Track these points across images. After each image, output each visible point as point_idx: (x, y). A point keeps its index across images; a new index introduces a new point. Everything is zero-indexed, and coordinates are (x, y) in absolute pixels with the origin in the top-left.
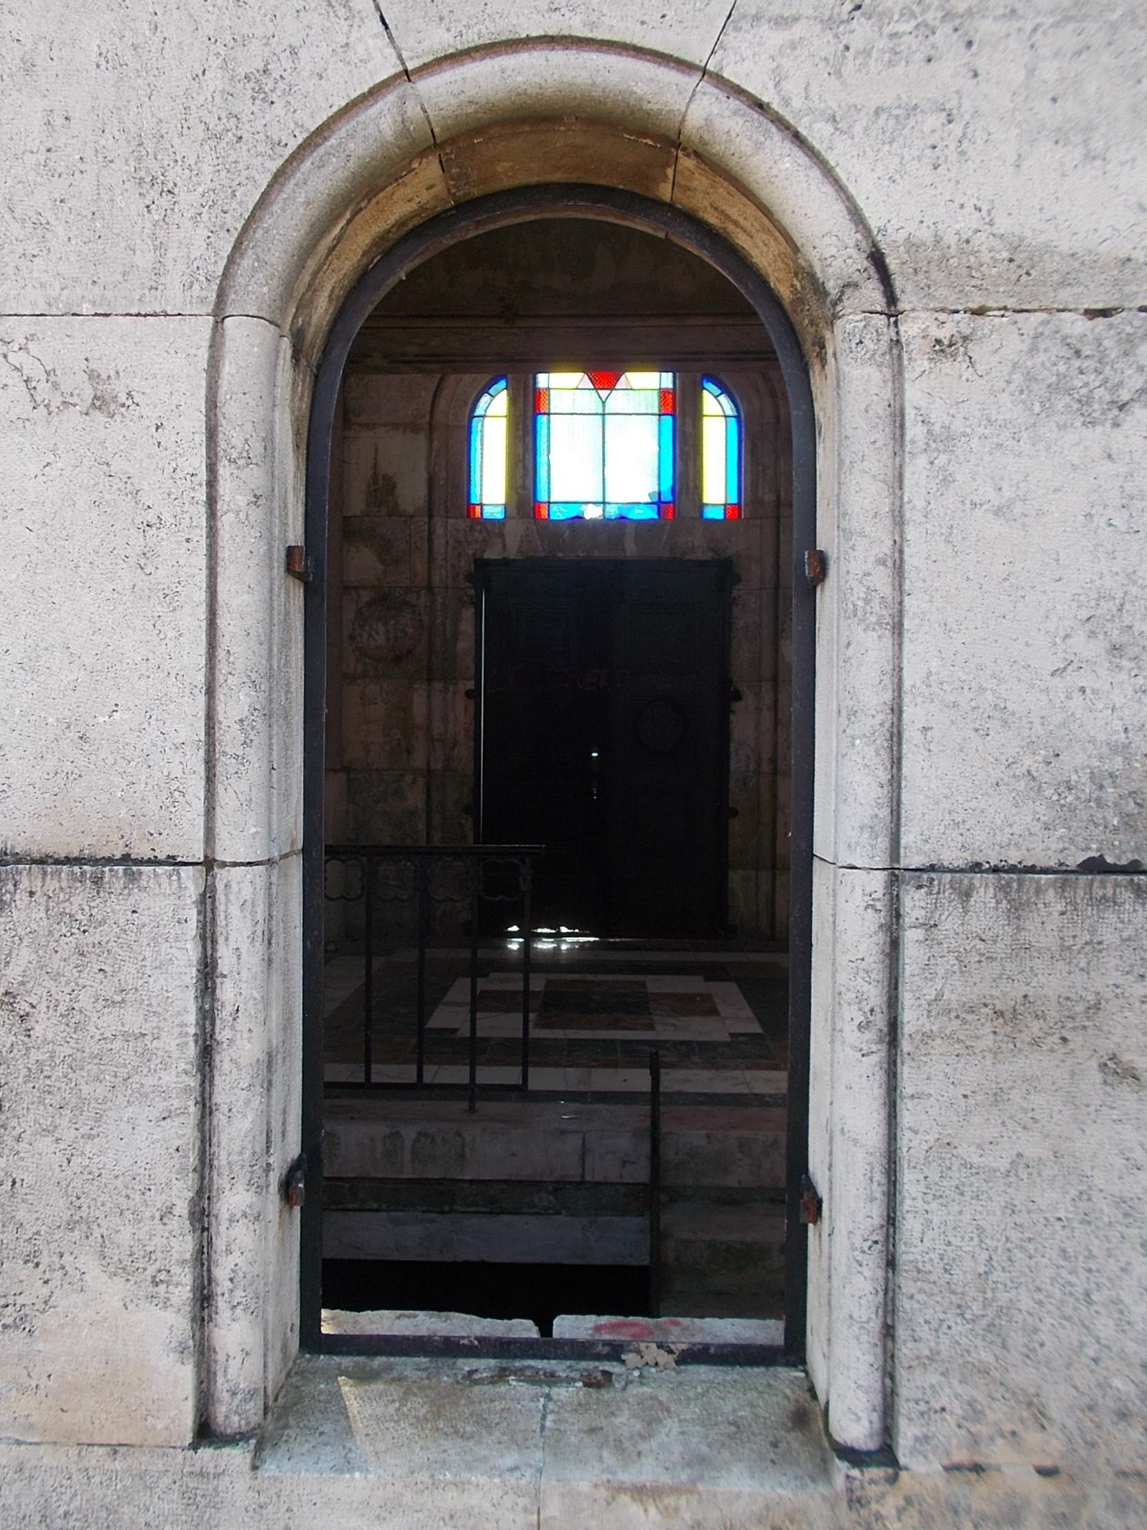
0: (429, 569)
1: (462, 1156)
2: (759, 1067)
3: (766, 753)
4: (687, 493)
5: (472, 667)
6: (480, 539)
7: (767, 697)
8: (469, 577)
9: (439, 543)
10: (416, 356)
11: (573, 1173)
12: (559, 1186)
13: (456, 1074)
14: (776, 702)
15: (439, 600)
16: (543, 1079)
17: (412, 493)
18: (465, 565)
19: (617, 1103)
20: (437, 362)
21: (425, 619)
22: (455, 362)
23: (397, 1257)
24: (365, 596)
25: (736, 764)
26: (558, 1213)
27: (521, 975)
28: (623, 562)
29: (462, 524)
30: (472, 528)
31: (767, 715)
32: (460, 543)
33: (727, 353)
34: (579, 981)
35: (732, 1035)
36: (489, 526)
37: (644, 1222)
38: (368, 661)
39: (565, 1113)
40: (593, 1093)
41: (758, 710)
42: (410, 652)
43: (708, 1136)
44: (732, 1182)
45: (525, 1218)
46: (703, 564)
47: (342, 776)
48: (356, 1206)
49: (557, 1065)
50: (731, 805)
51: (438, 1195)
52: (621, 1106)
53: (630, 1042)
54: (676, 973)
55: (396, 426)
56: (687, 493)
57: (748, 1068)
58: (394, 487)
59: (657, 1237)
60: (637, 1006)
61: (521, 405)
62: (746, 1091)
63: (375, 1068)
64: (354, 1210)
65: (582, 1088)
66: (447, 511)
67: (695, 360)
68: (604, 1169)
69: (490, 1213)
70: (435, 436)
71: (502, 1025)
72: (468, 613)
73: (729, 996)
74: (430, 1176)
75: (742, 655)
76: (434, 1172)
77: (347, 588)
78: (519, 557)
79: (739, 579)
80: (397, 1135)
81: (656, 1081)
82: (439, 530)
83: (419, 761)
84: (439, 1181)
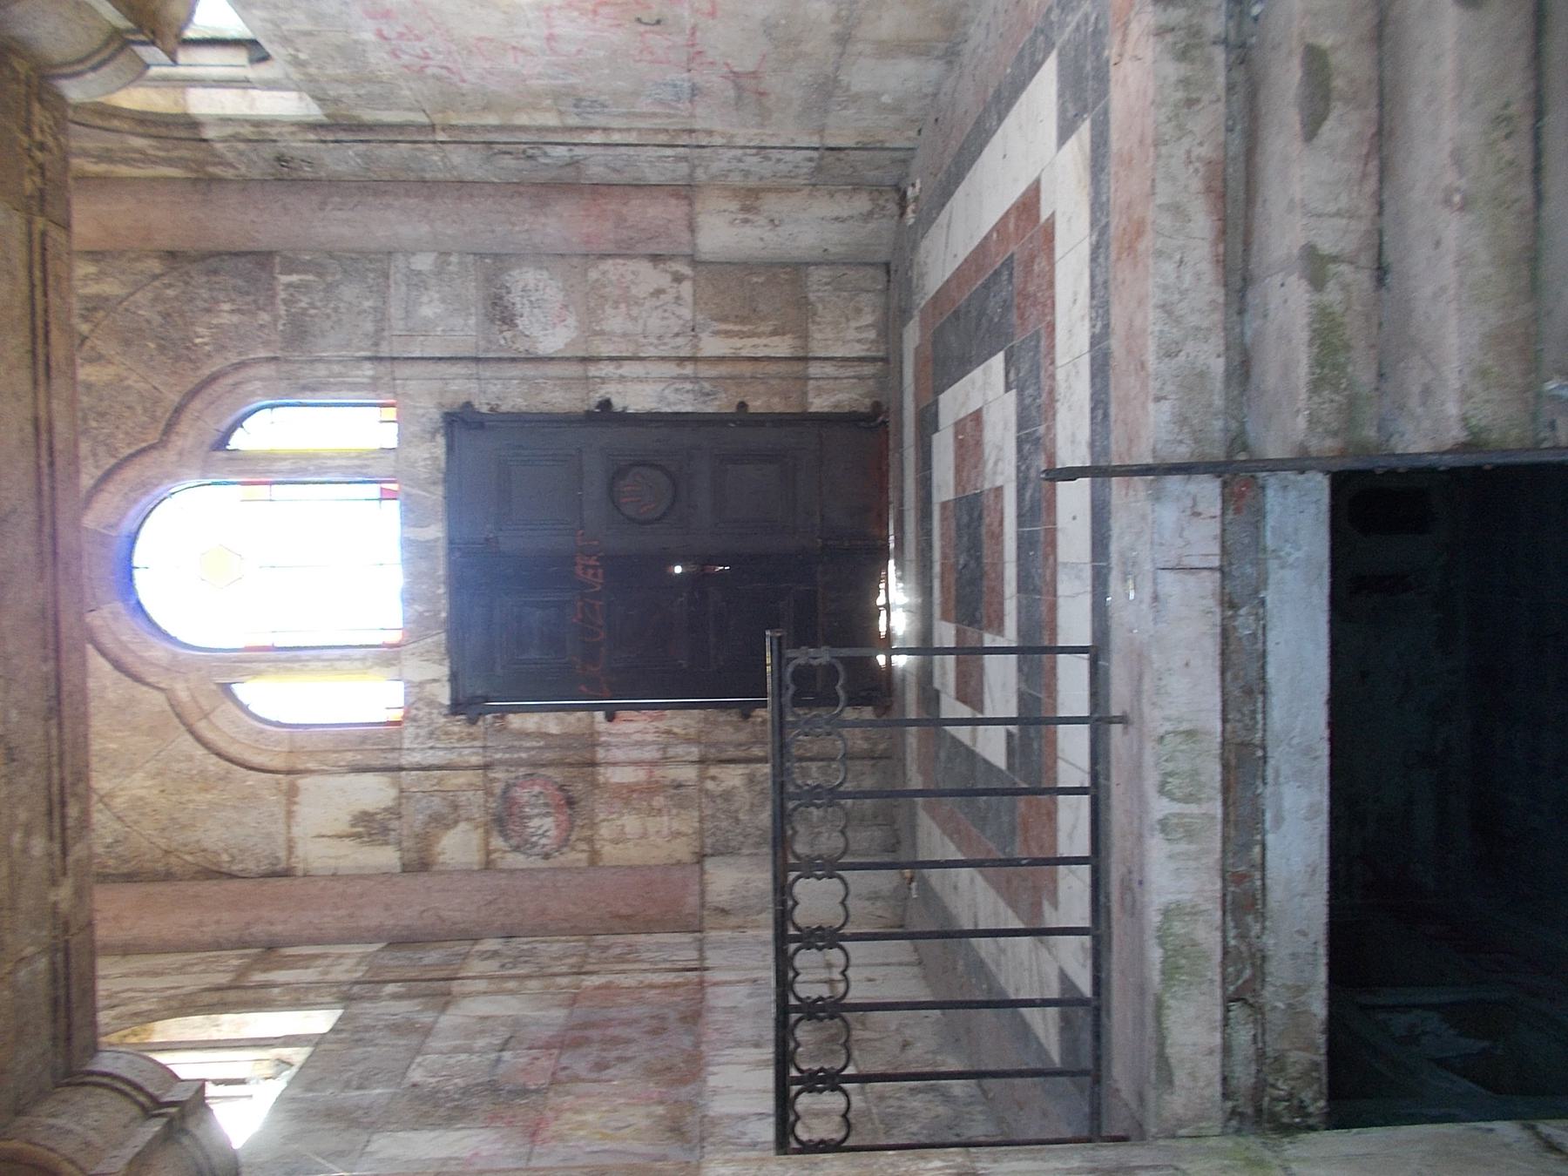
0: (466, 768)
1: (1190, 734)
2: (1052, 347)
3: (672, 369)
4: (366, 466)
5: (579, 714)
6: (427, 710)
7: (608, 369)
8: (472, 722)
9: (438, 757)
10: (51, 838)
11: (1211, 581)
12: (1229, 603)
13: (1073, 745)
14: (611, 359)
15: (498, 756)
16: (1074, 625)
17: (374, 792)
18: (458, 726)
19: (1109, 529)
20: (63, 804)
21: (522, 771)
22: (62, 780)
23: (1324, 818)
24: (497, 842)
25: (686, 404)
26: (1263, 602)
27: (937, 657)
28: (451, 542)
29: (409, 731)
30: (414, 720)
31: (628, 369)
32: (431, 733)
33: (35, 382)
34: (942, 581)
35: (1008, 388)
36: (412, 700)
37: (1272, 482)
38: (573, 837)
39: (1121, 594)
40: (1093, 561)
41: (622, 379)
42: (561, 788)
43: (1158, 399)
44: (1218, 366)
45: (1270, 646)
46: (450, 448)
47: (709, 864)
48: (1258, 875)
49: (1053, 608)
50: (733, 410)
51: (1243, 763)
52: (1112, 521)
53: (1020, 516)
54: (930, 468)
55: (290, 814)
56: (366, 466)
57: (1053, 363)
58: (365, 813)
59: (1300, 463)
60: (972, 512)
61: (263, 666)
62: (1086, 359)
63: (1064, 850)
64: (1263, 879)
65: (1087, 573)
66: (393, 749)
67: (50, 430)
68: (1203, 543)
69: (1264, 692)
70: (301, 767)
71: (1001, 683)
72: (515, 721)
73: (953, 404)
74: (1218, 778)
75: (560, 399)
76: (1213, 771)
77: (488, 865)
78: (447, 662)
79: (468, 405)
80: (1164, 825)
81: (1072, 474)
82: (416, 758)
83: (689, 774)
84: (1226, 767)
